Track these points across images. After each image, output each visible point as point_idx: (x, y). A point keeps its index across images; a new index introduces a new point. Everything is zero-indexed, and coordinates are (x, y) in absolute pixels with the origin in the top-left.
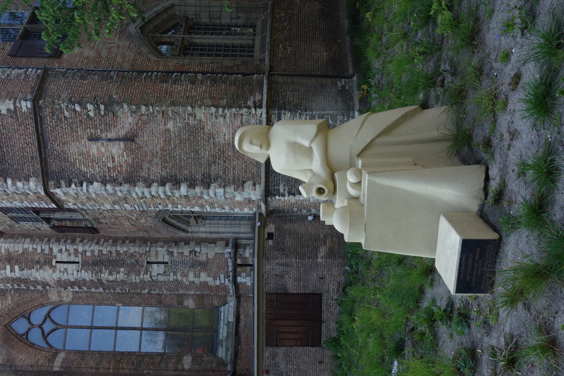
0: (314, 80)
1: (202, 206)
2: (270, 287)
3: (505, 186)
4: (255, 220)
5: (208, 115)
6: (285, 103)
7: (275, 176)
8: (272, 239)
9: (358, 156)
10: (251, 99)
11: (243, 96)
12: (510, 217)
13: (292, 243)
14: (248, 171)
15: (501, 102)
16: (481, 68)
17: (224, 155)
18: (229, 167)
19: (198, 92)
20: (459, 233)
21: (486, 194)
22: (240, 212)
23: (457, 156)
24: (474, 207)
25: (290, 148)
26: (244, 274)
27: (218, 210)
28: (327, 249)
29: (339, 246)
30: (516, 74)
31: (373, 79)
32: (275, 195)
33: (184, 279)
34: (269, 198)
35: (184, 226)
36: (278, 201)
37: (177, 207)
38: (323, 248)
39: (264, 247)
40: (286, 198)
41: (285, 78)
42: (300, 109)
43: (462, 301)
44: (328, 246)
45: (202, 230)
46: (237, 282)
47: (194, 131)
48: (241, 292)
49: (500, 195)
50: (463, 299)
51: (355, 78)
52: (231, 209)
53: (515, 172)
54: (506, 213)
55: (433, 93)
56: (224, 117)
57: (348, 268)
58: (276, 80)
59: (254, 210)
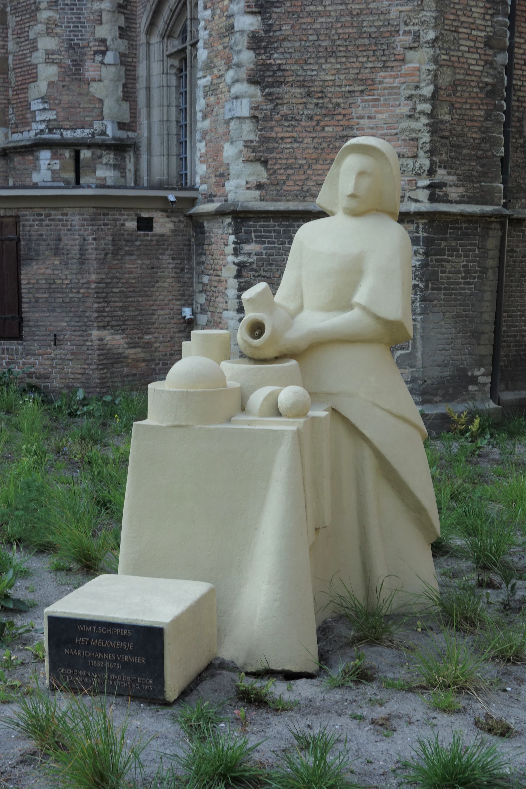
0: (489, 316)
1: (209, 66)
2: (31, 226)
3: (277, 710)
4: (180, 189)
5: (416, 79)
6: (441, 252)
7: (278, 232)
8: (139, 228)
9: (333, 409)
10: (451, 178)
11: (457, 159)
12: (212, 721)
13: (132, 272)
14: (290, 171)
15: (452, 699)
16: (521, 660)
17: (325, 115)
18: (299, 129)
19: (467, 55)
20: (176, 621)
21: (257, 675)
22: (198, 154)
23: (334, 615)
24: (228, 653)
25: (349, 261)
26: (57, 165)
27: (201, 103)
28: (121, 351)
29: (127, 376)
30: (509, 728)
31: (489, 444)
32: (236, 232)
33: (40, 27)
34: (229, 220)
35: (161, 24)
36: (222, 239)
37: (205, 8)
38: (122, 342)
39: (120, 209)
40: (231, 259)
41: (494, 253)
42: (426, 286)
43: (28, 631)
44: (128, 352)
45: (154, 67)
46: (38, 151)
47: (380, 47)
48: (17, 159)
49: (257, 701)
50: (33, 633)
51: (492, 405)
52: (205, 134)
53: (307, 731)
54: (220, 713)
55: (464, 565)
56: (410, 117)
57: (80, 395)
58: (491, 233)
59: (203, 188)
